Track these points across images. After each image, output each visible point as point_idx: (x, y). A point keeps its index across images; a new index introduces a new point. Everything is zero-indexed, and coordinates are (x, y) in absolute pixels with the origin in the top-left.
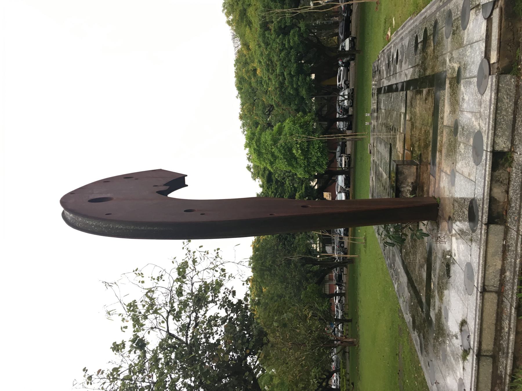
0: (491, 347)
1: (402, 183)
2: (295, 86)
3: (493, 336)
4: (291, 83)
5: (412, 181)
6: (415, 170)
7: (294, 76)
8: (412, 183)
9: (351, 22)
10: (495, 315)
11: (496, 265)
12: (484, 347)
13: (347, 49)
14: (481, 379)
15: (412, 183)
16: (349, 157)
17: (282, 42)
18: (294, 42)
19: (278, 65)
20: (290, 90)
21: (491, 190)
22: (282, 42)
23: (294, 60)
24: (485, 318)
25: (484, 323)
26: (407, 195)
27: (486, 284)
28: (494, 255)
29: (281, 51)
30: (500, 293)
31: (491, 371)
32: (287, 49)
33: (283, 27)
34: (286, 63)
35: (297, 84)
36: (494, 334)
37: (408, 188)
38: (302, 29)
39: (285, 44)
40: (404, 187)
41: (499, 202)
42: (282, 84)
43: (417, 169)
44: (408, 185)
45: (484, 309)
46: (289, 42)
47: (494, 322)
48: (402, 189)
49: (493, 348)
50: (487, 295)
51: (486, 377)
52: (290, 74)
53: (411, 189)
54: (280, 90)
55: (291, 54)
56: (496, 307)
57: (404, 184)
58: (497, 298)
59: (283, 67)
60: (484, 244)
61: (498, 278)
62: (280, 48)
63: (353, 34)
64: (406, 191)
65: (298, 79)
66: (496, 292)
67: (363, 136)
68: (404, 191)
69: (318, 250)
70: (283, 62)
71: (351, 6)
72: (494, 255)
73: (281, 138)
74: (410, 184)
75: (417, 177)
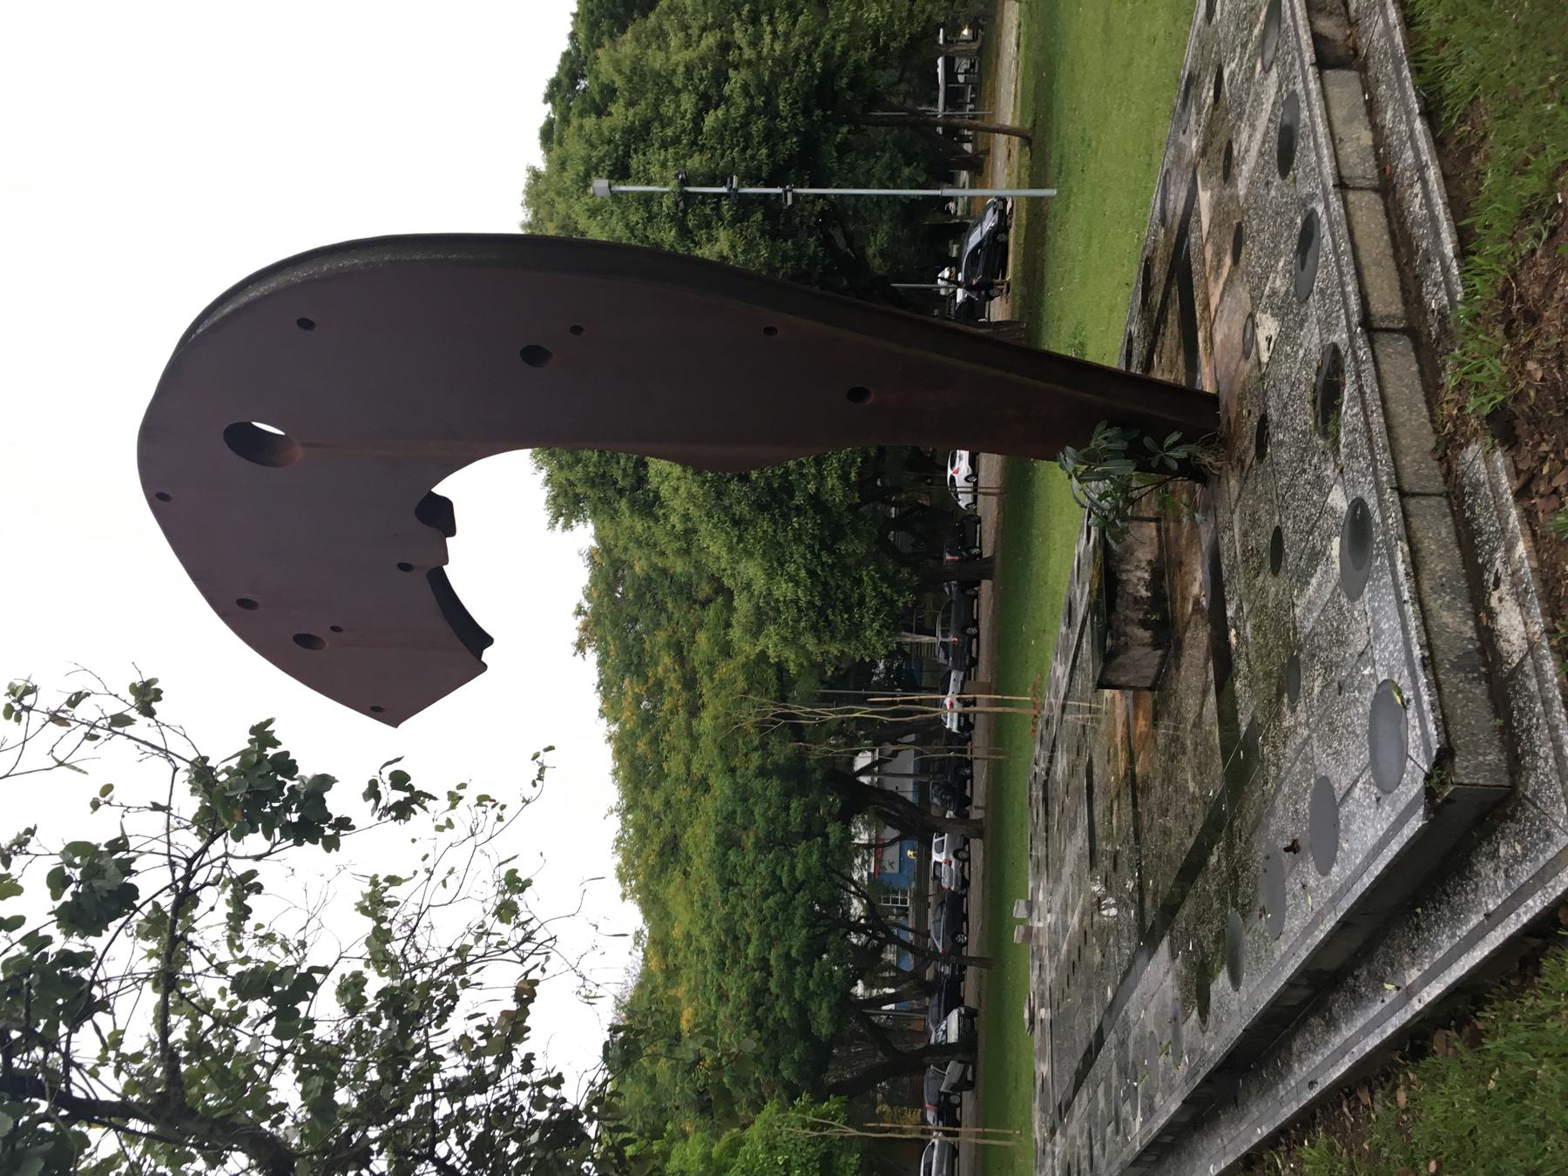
0: (1397, 308)
1: (1121, 560)
2: (797, 994)
3: (1397, 285)
4: (787, 986)
5: (1149, 557)
6: (1154, 533)
7: (797, 963)
8: (1150, 562)
9: (966, 917)
10: (1386, 237)
11: (1358, 139)
12: (1378, 307)
13: (953, 1037)
14: (1390, 390)
15: (1150, 562)
16: (968, 1018)
17: (773, 872)
18: (808, 870)
19: (754, 937)
20: (782, 1009)
21: (1311, 23)
22: (773, 872)
23: (803, 918)
24: (1364, 244)
25: (1362, 253)
26: (1138, 591)
27: (1345, 172)
28: (1350, 120)
29: (766, 895)
30: (1387, 188)
31: (1415, 368)
32: (783, 890)
33: (779, 834)
34: (777, 927)
35: (806, 988)
36: (1395, 275)
37: (1139, 573)
38: (832, 841)
39: (780, 880)
40: (1128, 571)
41: (1334, 41)
42: (758, 994)
43: (1159, 530)
44: (1138, 567)
45: (1354, 224)
46: (793, 868)
47: (1389, 252)
48: (1124, 577)
49: (1405, 311)
50: (1352, 196)
51: (1407, 386)
52: (788, 955)
53: (1146, 576)
54: (752, 1013)
55: (796, 903)
56: (1383, 221)
57: (1127, 563)
58: (1380, 201)
59: (769, 941)
60: (1320, 97)
61: (1372, 161)
62: (766, 886)
63: (970, 1000)
64: (1135, 580)
65: (810, 975)
66: (1376, 190)
67: (1011, 706)
68: (1128, 581)
69: (875, 679)
70: (768, 926)
71: (958, 1110)
72: (1350, 120)
73: (733, 1164)
74: (1144, 564)
75: (1160, 548)
